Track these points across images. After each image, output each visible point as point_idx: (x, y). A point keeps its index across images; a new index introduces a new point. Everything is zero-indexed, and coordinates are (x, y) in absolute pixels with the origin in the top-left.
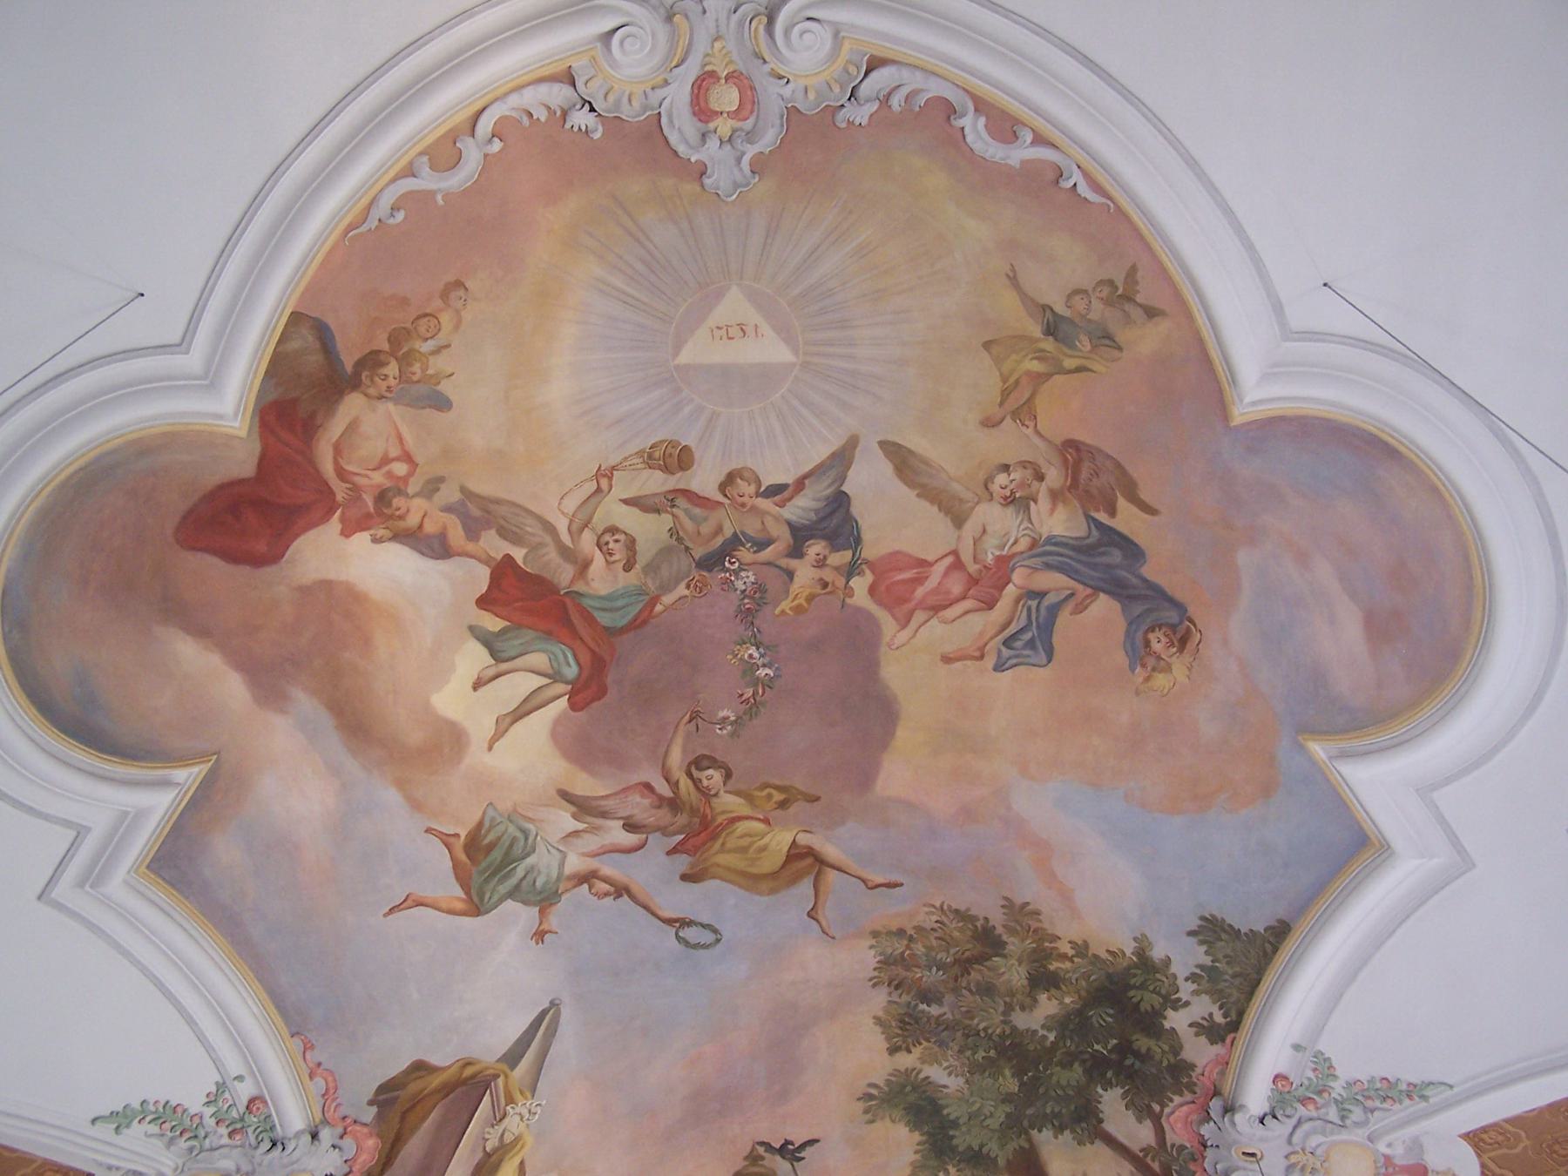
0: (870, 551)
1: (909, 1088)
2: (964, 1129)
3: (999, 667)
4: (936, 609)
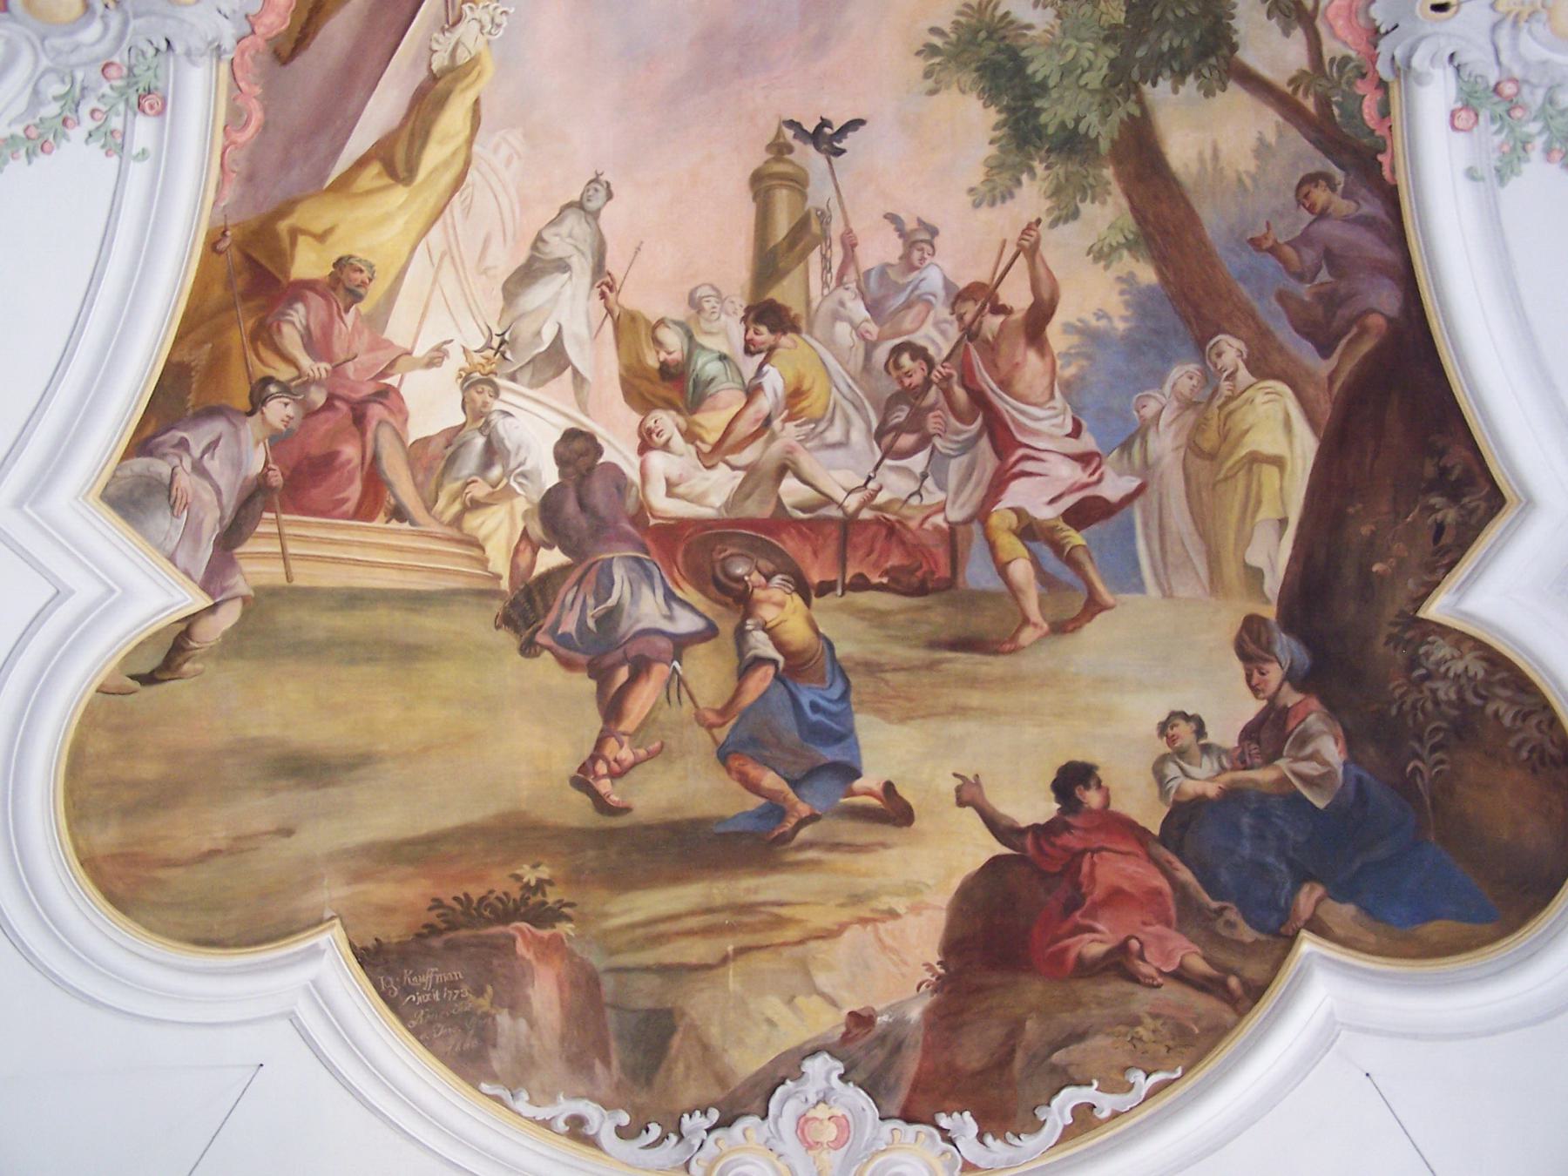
1: (983, 35)
2: (1054, 94)
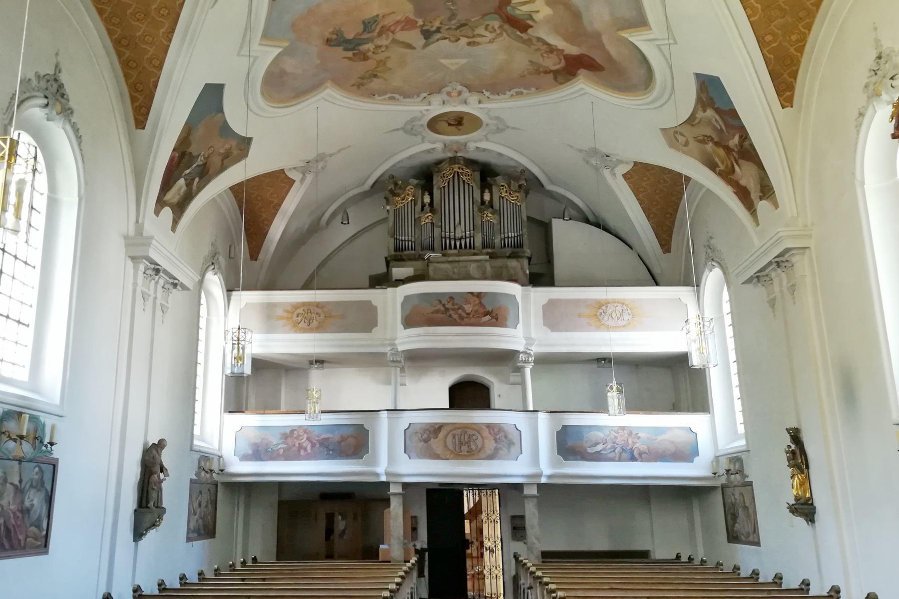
0: (419, 30)
3: (378, 16)
4: (398, 22)
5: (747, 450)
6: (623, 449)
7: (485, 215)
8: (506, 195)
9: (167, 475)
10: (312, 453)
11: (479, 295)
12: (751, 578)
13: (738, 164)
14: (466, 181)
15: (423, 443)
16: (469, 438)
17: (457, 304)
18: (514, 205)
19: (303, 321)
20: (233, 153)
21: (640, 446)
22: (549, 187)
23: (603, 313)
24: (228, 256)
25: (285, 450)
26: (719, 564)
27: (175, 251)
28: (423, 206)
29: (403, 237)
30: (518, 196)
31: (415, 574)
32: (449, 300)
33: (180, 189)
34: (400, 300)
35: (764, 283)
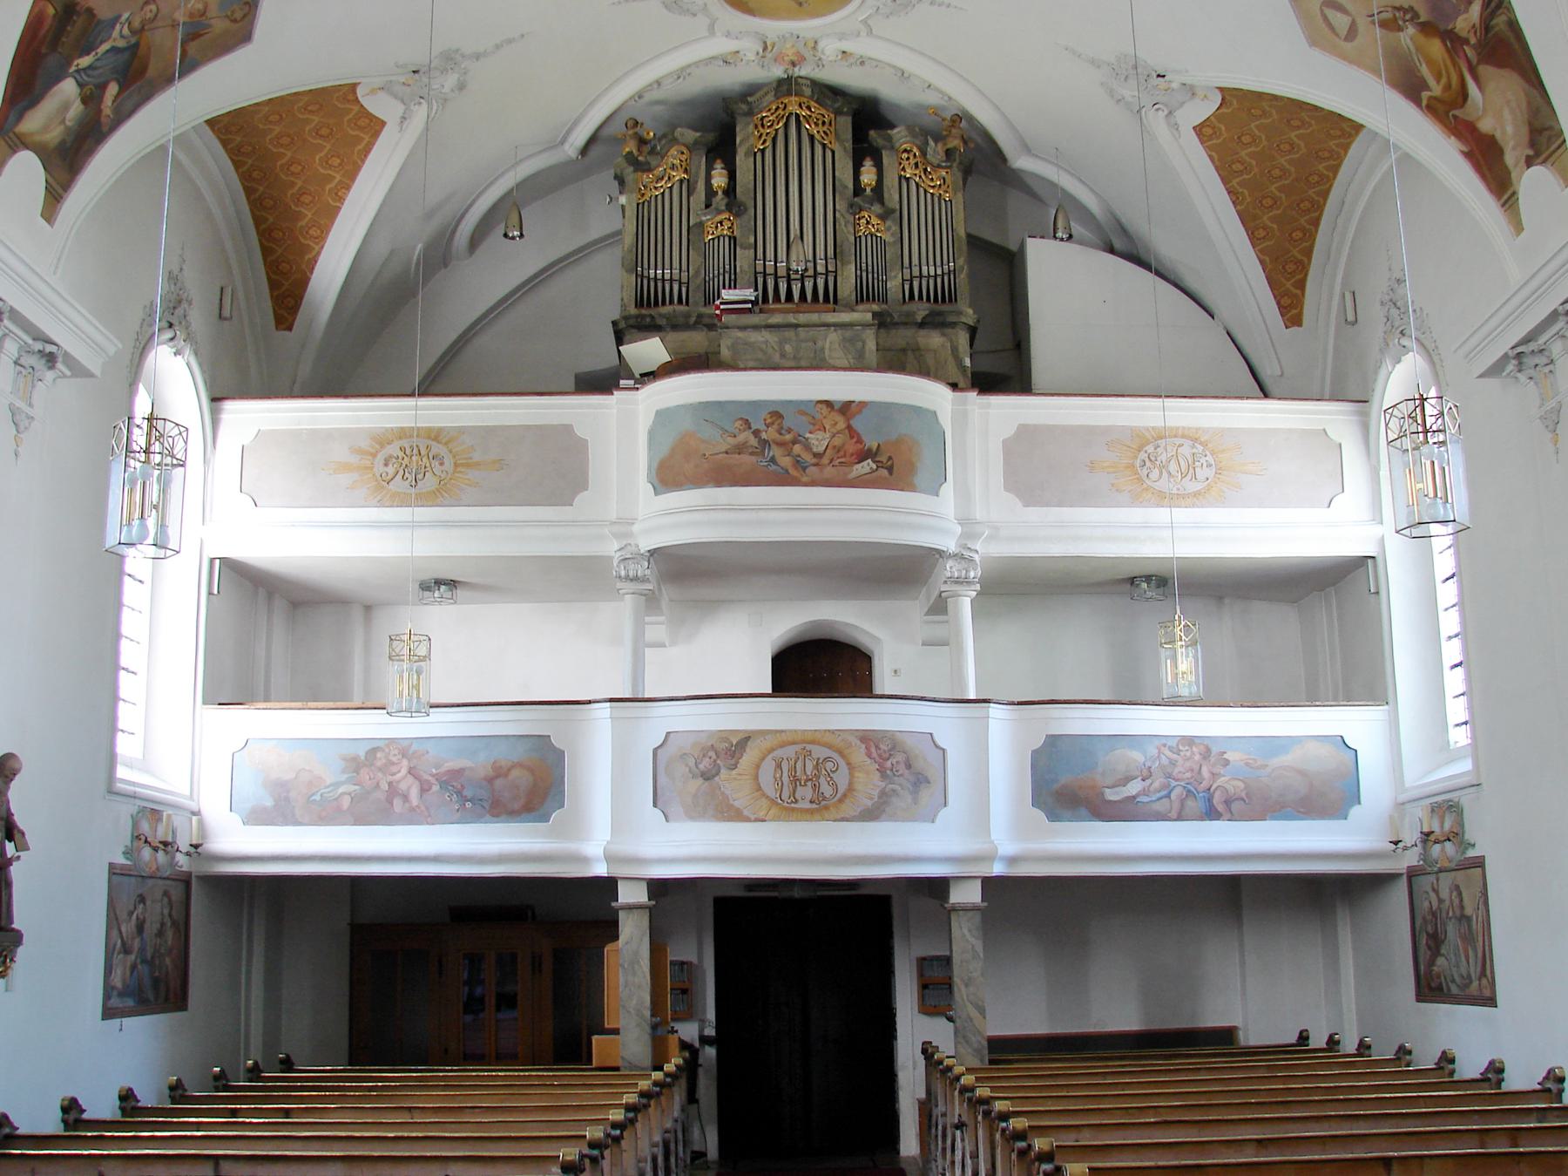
5: (1475, 783)
6: (1189, 791)
7: (863, 221)
8: (916, 175)
9: (22, 847)
10: (423, 808)
11: (846, 409)
12: (1484, 1079)
13: (1476, 79)
14: (817, 137)
15: (700, 781)
16: (816, 767)
17: (789, 431)
18: (936, 199)
19: (399, 476)
20: (210, 26)
21: (1228, 782)
22: (1021, 162)
23: (1148, 463)
24: (218, 315)
25: (354, 799)
26: (1403, 1052)
27: (55, 273)
28: (710, 193)
29: (659, 272)
30: (944, 179)
31: (678, 1096)
32: (769, 421)
33: (66, 107)
34: (644, 422)
35: (1531, 372)
